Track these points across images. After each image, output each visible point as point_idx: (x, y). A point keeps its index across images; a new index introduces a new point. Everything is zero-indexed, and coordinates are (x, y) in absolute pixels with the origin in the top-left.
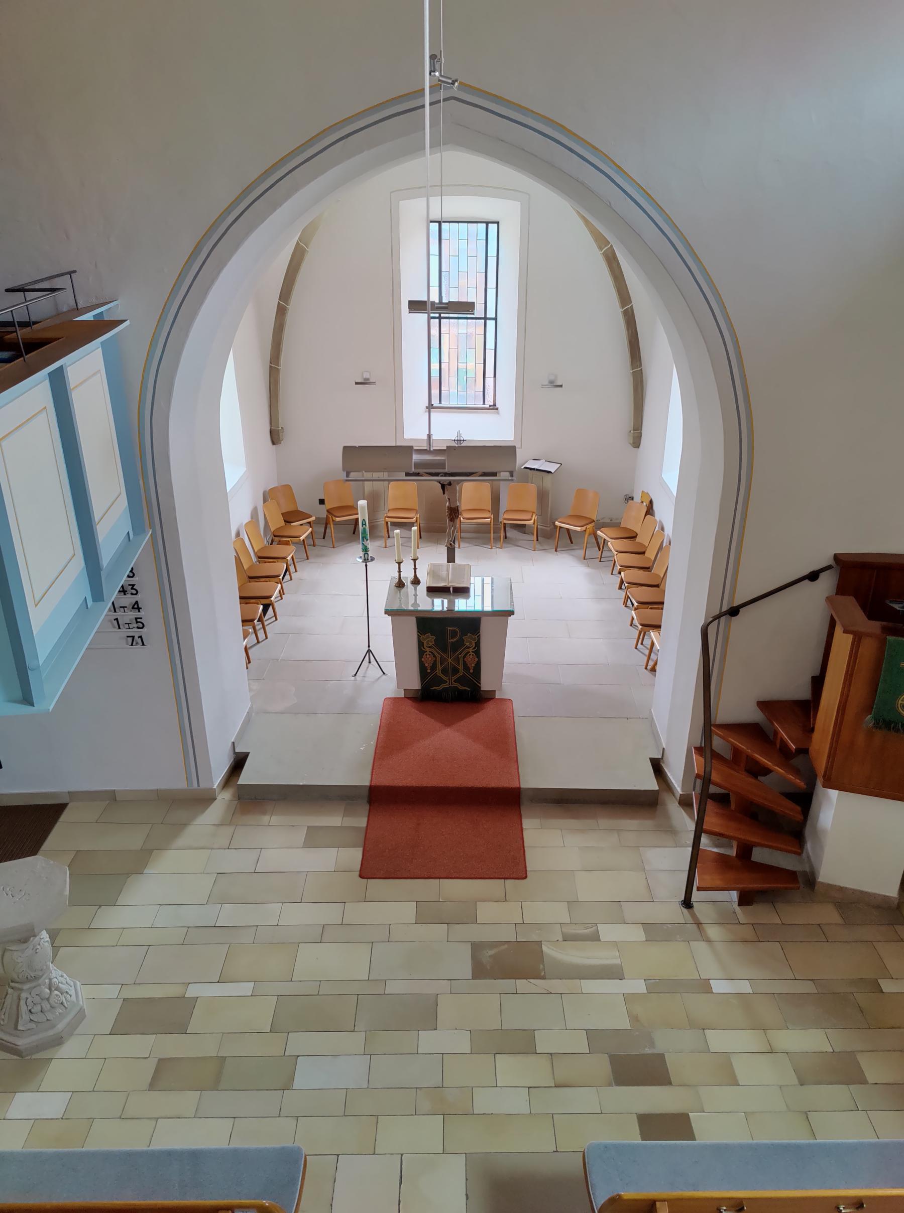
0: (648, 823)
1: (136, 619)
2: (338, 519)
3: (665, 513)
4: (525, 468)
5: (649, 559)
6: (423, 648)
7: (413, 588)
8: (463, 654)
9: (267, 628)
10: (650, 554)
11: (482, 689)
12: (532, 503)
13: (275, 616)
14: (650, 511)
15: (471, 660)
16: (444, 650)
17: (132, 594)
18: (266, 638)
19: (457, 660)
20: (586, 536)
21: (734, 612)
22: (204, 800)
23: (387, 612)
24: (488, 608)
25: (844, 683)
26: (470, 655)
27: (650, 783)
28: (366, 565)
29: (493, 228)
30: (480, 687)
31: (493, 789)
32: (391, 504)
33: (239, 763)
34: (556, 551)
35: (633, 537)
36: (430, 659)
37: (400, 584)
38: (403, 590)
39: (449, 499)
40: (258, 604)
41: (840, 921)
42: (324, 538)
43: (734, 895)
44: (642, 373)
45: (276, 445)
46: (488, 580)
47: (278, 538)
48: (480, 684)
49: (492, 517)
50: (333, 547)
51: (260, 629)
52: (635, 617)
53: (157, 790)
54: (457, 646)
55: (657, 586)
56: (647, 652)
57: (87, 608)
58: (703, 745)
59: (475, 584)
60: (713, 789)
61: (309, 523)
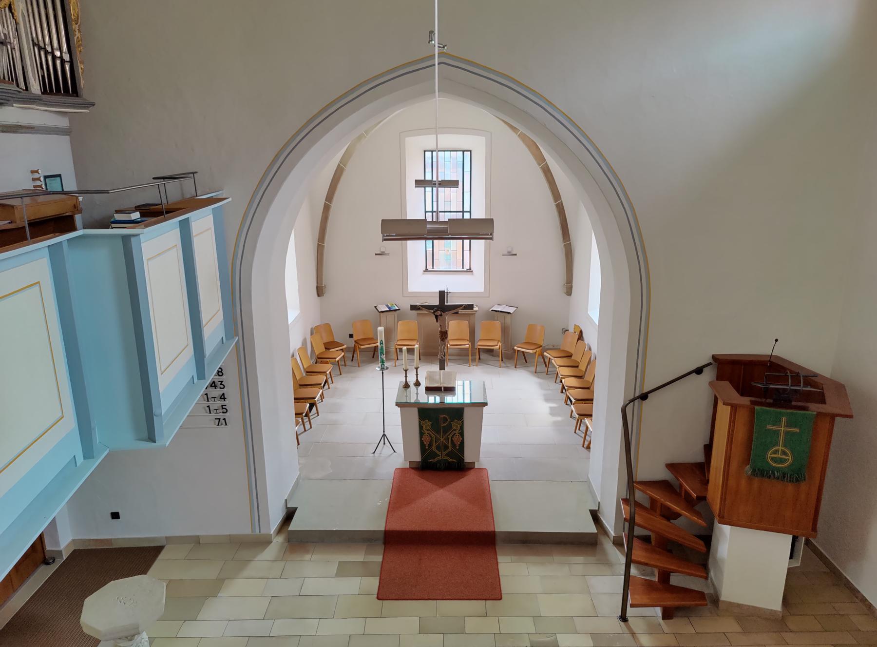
0: (591, 559)
1: (222, 406)
2: (362, 347)
3: (591, 338)
4: (492, 310)
5: (582, 371)
7: (415, 388)
8: (451, 436)
9: (312, 421)
10: (582, 367)
11: (465, 461)
12: (498, 334)
13: (318, 413)
14: (581, 337)
16: (438, 432)
17: (221, 388)
18: (311, 428)
20: (536, 356)
21: (644, 397)
22: (263, 542)
23: (398, 404)
24: (467, 401)
25: (727, 445)
27: (592, 529)
28: (383, 373)
29: (467, 154)
30: (464, 460)
31: (475, 532)
32: (399, 337)
33: (289, 516)
34: (515, 367)
35: (569, 356)
37: (407, 386)
38: (408, 390)
39: (441, 325)
40: (306, 403)
41: (739, 629)
42: (352, 361)
43: (658, 611)
44: (571, 245)
45: (321, 297)
46: (467, 383)
47: (320, 359)
48: (464, 457)
49: (470, 344)
50: (359, 367)
51: (307, 422)
52: (574, 410)
53: (230, 535)
55: (588, 388)
56: (583, 435)
57: (194, 383)
58: (628, 497)
59: (458, 385)
60: (638, 531)
61: (342, 349)
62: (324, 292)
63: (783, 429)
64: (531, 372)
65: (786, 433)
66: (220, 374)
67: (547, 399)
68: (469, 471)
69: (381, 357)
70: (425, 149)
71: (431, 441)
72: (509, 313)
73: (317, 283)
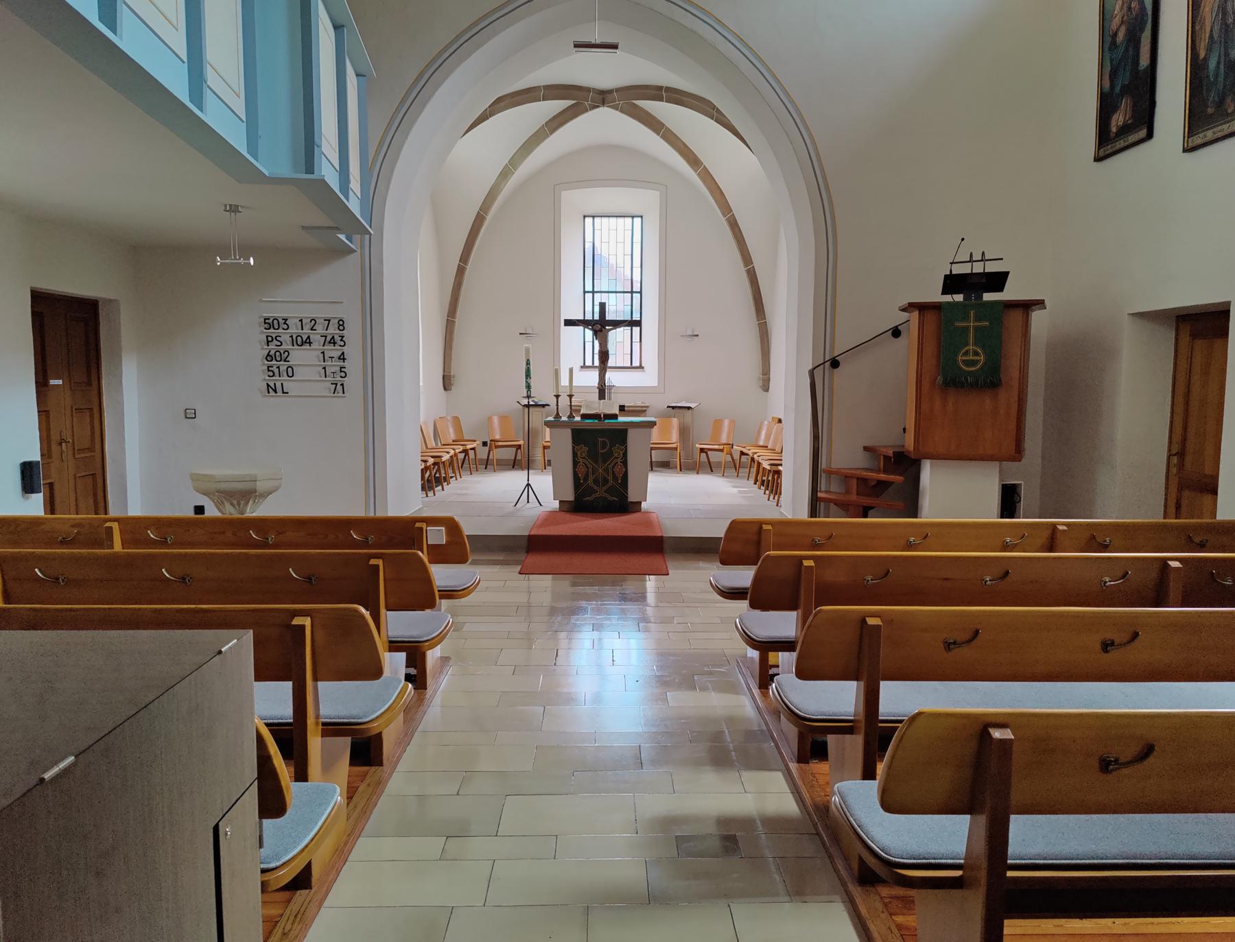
4: (668, 407)
11: (629, 500)
16: (596, 462)
19: (606, 470)
44: (766, 325)
45: (449, 392)
54: (607, 457)
62: (452, 383)
63: (972, 324)
65: (976, 328)
66: (341, 328)
69: (527, 382)
71: (588, 472)
72: (689, 408)
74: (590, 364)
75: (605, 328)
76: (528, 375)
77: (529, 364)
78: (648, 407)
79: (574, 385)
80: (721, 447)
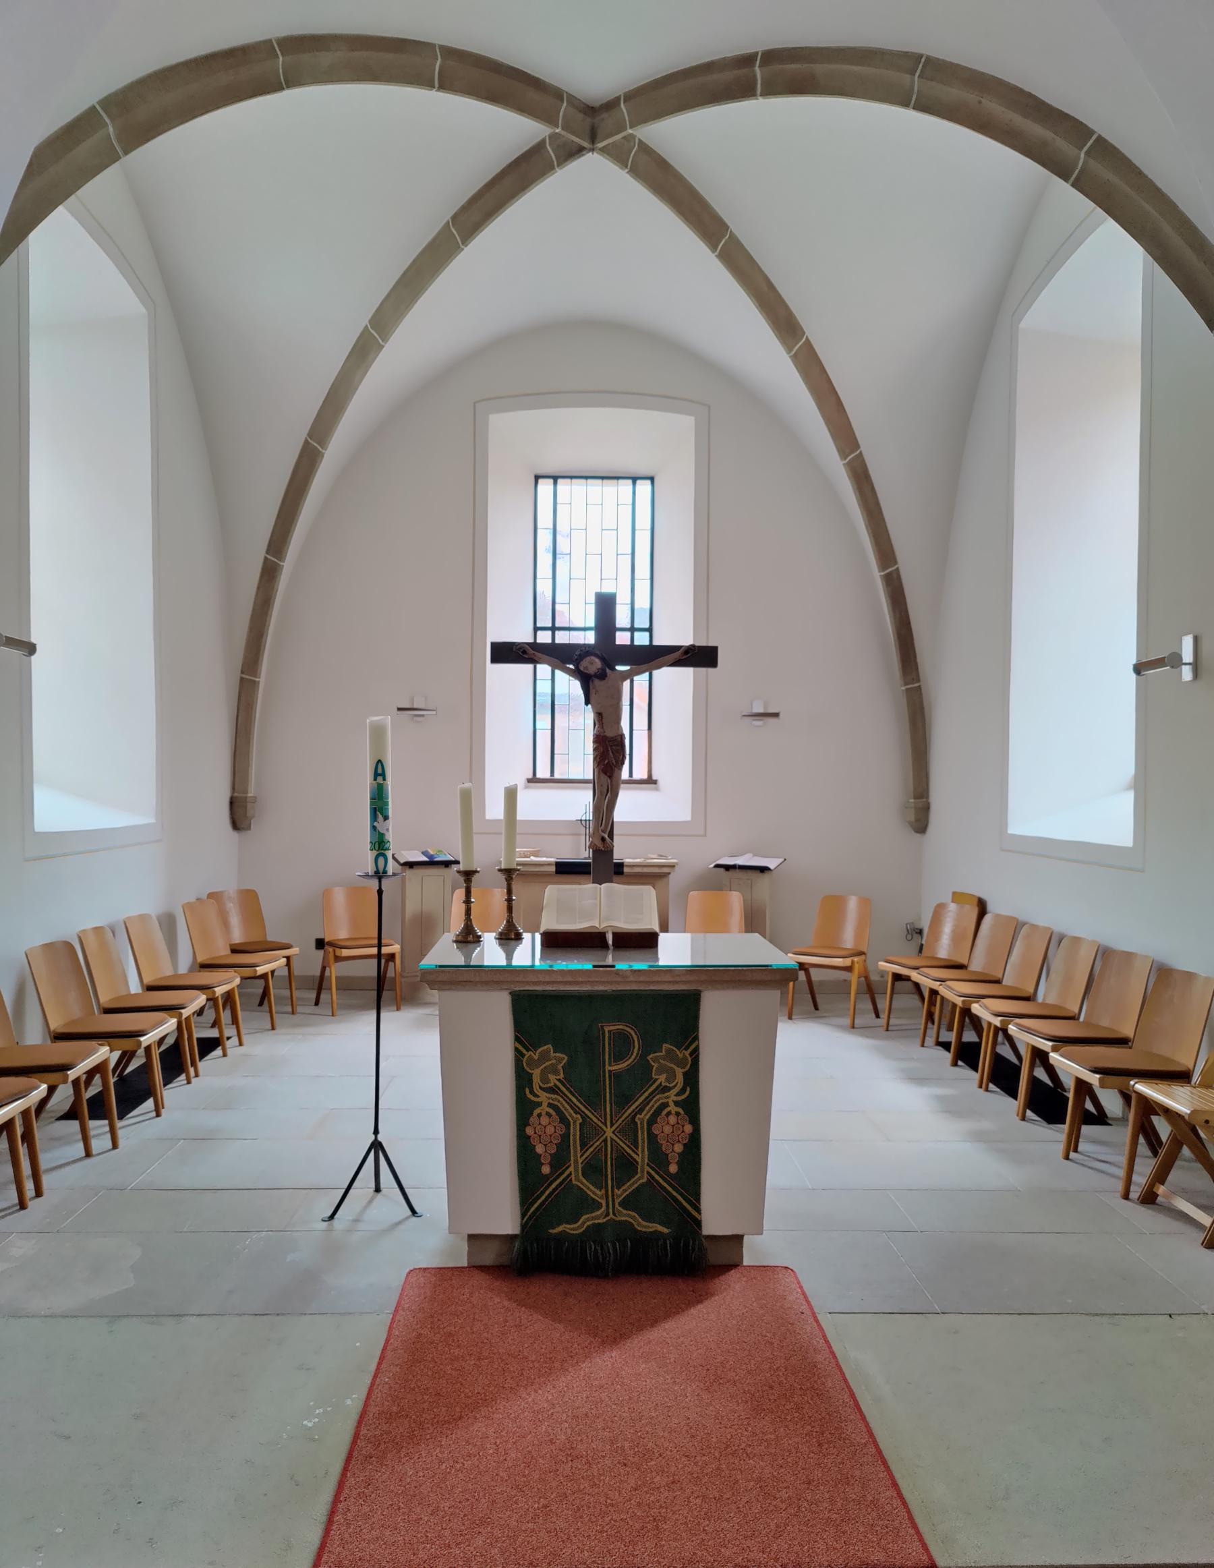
4: (717, 866)
6: (532, 1092)
8: (645, 1116)
15: (670, 1128)
16: (593, 1100)
19: (630, 1130)
26: (669, 1113)
30: (699, 1223)
36: (550, 1130)
44: (921, 694)
48: (699, 1211)
50: (333, 1016)
62: (249, 814)
64: (841, 1028)
67: (917, 1079)
68: (722, 1278)
69: (374, 828)
70: (540, 472)
71: (565, 1137)
72: (763, 870)
73: (233, 789)
74: (547, 775)
75: (613, 669)
76: (379, 808)
77: (383, 775)
78: (672, 866)
79: (519, 817)
80: (847, 962)
